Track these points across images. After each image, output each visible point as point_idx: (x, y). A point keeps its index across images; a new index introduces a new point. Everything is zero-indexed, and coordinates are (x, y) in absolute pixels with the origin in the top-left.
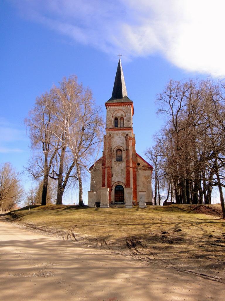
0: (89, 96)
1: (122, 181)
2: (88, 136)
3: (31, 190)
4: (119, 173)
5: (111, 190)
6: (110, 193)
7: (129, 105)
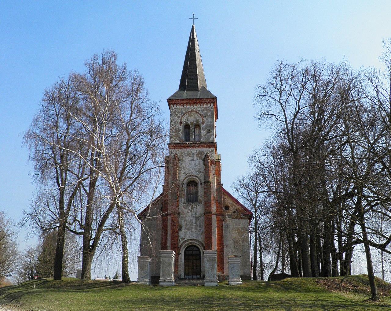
0: (138, 86)
1: (197, 239)
3: (29, 253)
4: (192, 225)
5: (178, 254)
6: (177, 260)
7: (210, 103)
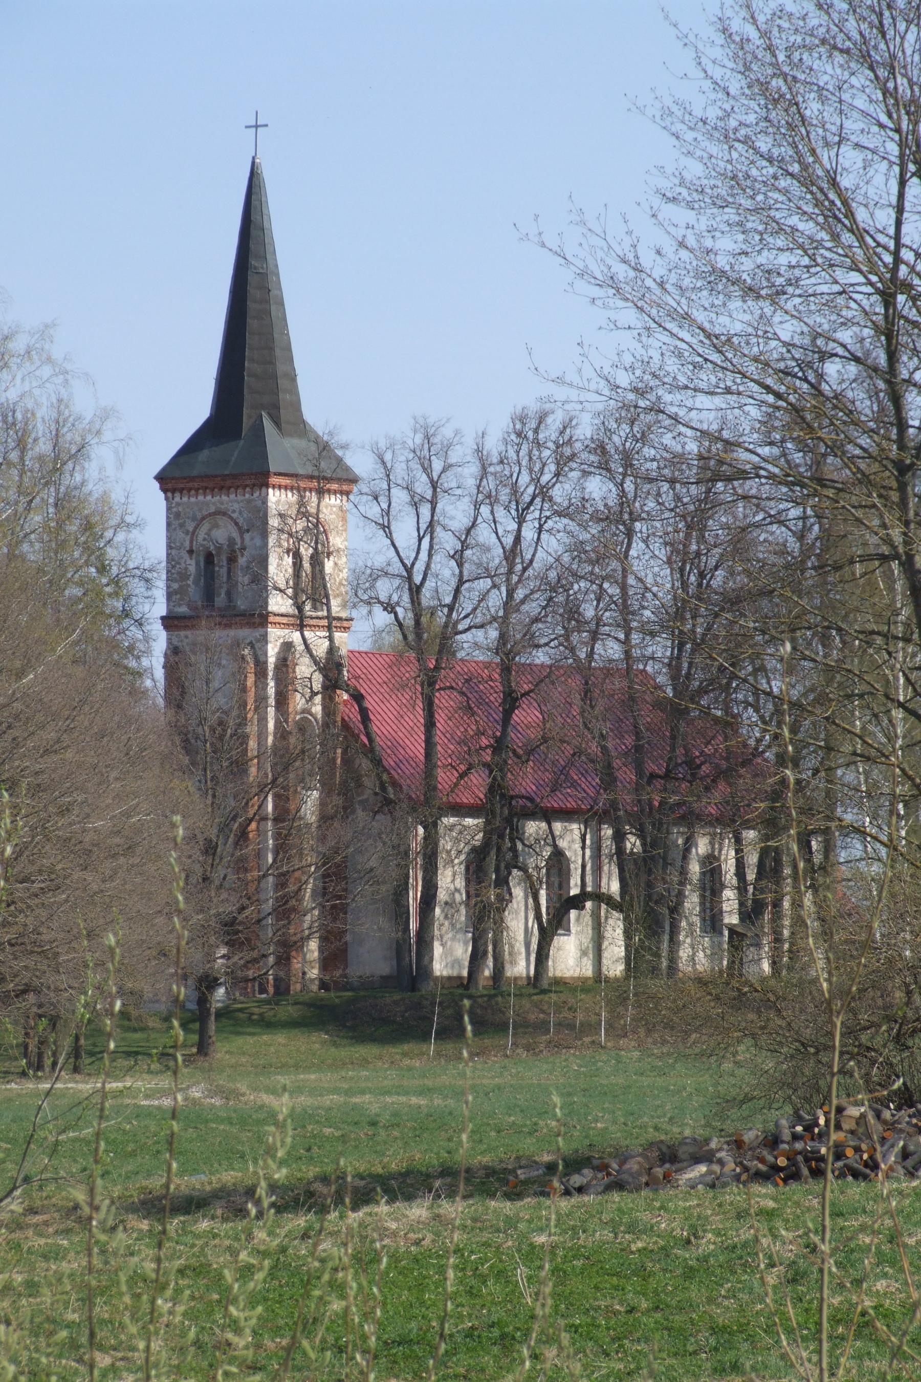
2: (911, 345)
